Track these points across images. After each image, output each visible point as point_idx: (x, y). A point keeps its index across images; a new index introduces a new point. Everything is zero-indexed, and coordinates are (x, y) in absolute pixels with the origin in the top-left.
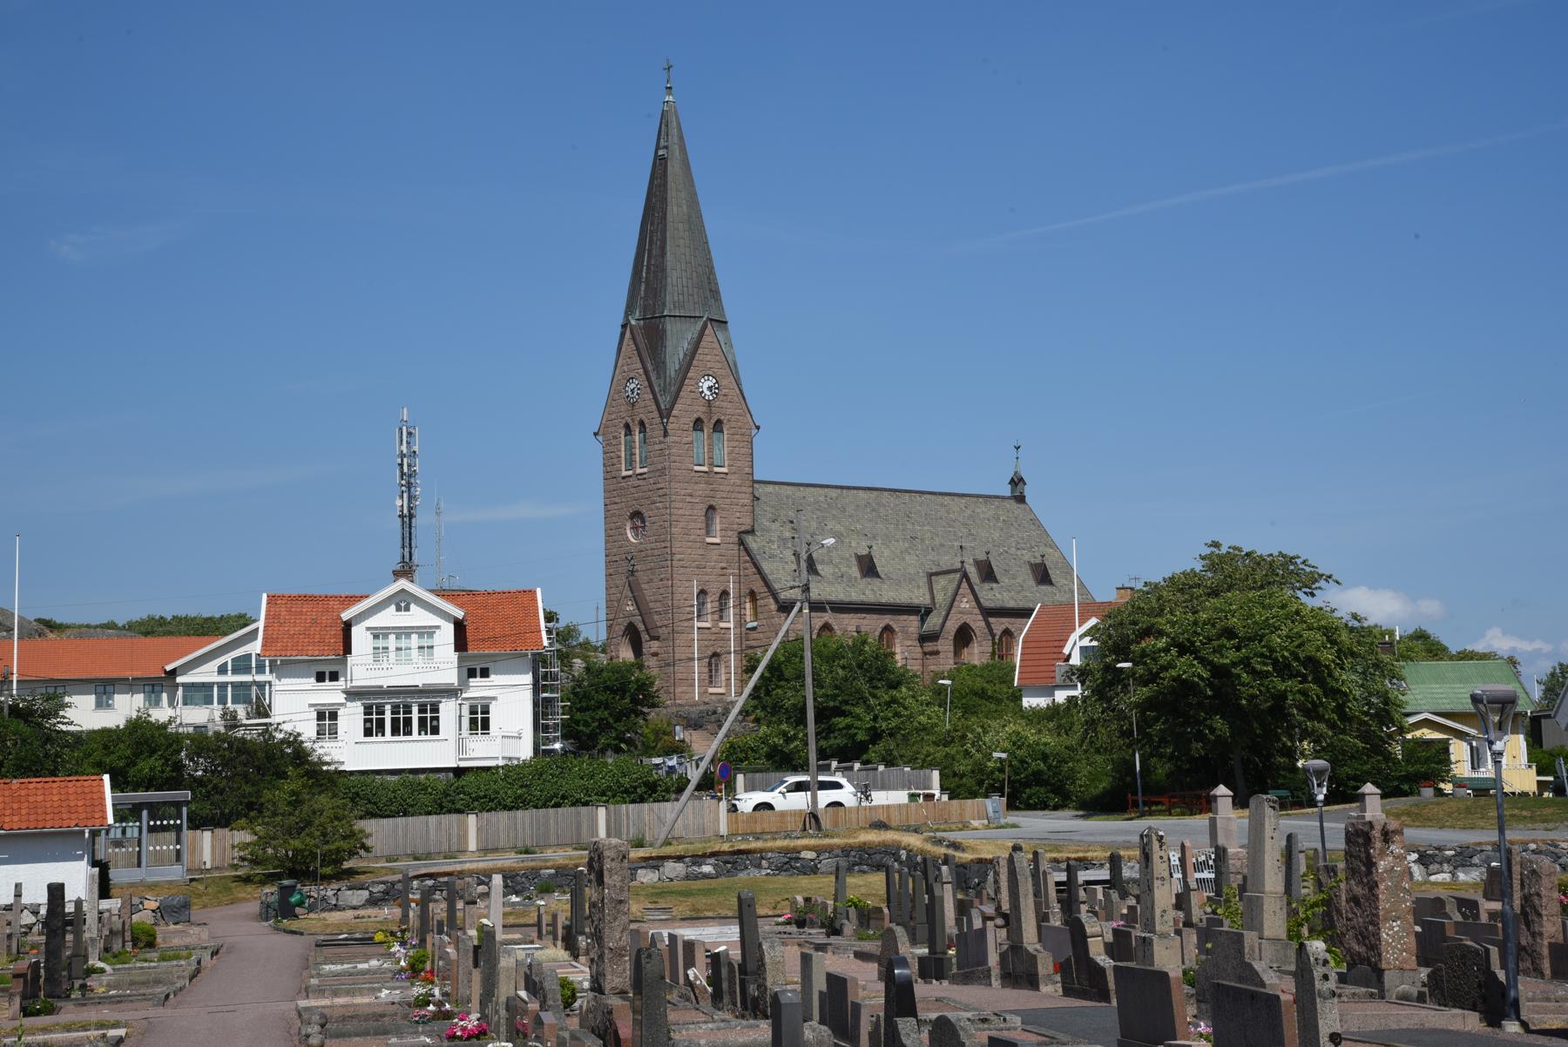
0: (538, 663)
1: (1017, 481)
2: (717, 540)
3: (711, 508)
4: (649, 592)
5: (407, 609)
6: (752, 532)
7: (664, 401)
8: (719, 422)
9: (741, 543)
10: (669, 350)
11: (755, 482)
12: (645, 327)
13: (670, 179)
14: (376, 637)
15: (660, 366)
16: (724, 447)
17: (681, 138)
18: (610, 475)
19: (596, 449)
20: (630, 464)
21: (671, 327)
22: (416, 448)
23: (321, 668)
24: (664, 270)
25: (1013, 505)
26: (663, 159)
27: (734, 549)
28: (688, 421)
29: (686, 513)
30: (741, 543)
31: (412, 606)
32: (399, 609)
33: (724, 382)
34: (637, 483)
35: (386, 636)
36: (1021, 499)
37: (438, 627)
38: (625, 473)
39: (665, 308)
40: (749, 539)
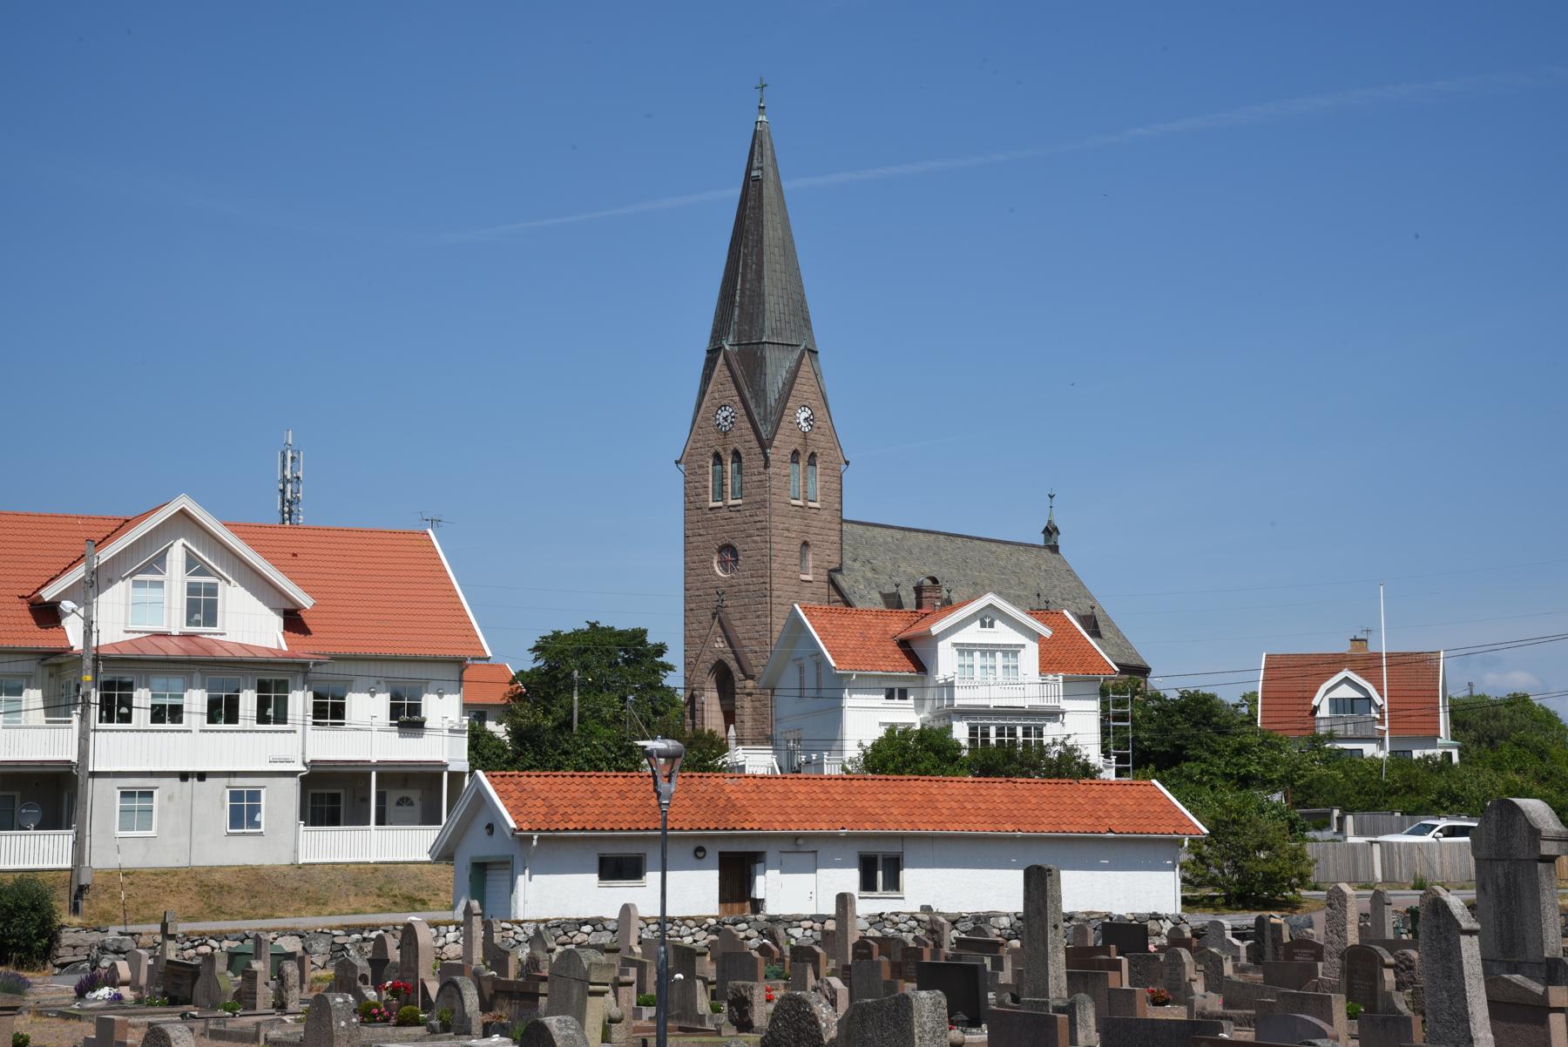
0: (1103, 693)
1: (1050, 531)
2: (809, 578)
3: (805, 544)
4: (740, 629)
5: (991, 625)
6: (839, 570)
7: (765, 431)
8: (813, 455)
9: (832, 582)
10: (769, 378)
11: (843, 521)
12: (739, 353)
13: (765, 201)
14: (961, 652)
15: (760, 394)
16: (817, 482)
17: (774, 160)
18: (693, 504)
19: (677, 479)
20: (720, 493)
21: (771, 354)
22: (300, 474)
23: (891, 685)
24: (761, 295)
25: (1047, 553)
26: (757, 180)
27: (824, 589)
28: (788, 452)
29: (783, 547)
30: (832, 582)
31: (997, 623)
32: (983, 625)
33: (818, 414)
34: (727, 514)
35: (971, 653)
36: (1054, 549)
37: (1023, 646)
38: (712, 504)
39: (751, 337)
40: (839, 577)
